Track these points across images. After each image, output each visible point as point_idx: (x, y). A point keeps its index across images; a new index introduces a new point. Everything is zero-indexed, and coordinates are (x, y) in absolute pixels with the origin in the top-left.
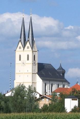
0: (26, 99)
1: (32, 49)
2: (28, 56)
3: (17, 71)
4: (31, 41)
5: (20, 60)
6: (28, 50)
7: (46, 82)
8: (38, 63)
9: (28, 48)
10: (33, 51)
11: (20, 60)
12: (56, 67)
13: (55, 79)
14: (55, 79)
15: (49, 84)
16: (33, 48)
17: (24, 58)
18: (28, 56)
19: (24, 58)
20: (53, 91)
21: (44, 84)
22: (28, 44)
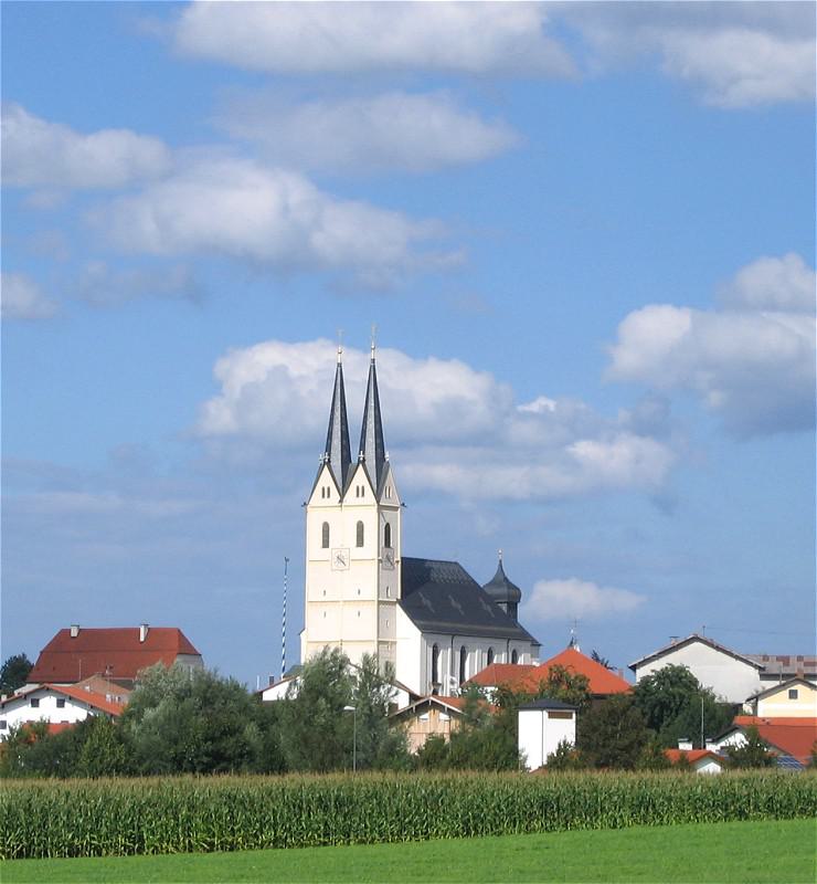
1: (378, 496)
2: (360, 527)
4: (371, 462)
5: (326, 544)
9: (360, 492)
10: (380, 508)
11: (326, 544)
15: (450, 650)
17: (343, 536)
18: (360, 527)
19: (343, 536)
22: (360, 479)
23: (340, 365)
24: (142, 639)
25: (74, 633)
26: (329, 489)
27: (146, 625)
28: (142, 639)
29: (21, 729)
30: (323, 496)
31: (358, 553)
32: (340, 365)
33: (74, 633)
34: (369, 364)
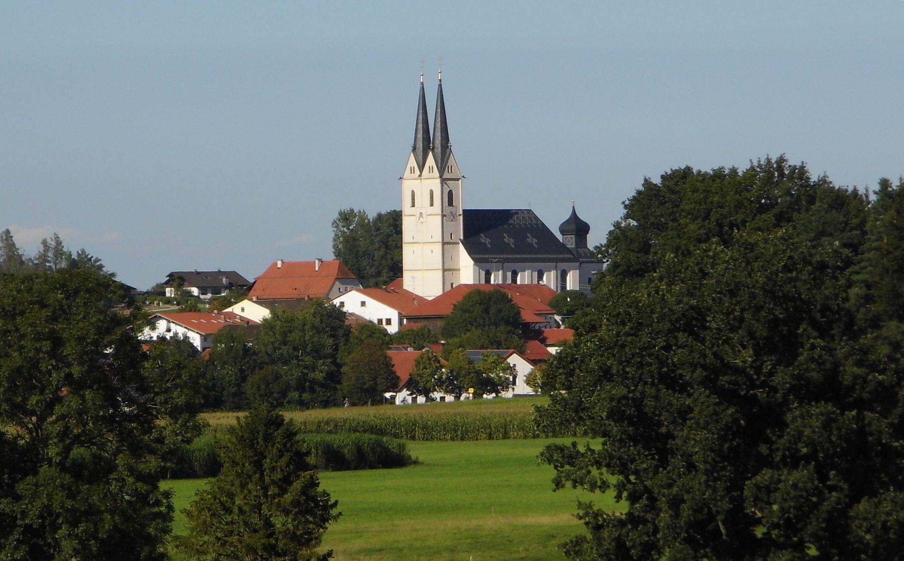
0: (493, 347)
1: (441, 171)
2: (432, 193)
3: (407, 236)
4: (438, 150)
5: (413, 205)
6: (431, 175)
7: (488, 266)
8: (464, 211)
9: (431, 170)
10: (443, 181)
11: (413, 205)
12: (678, 168)
13: (561, 256)
14: (561, 256)
15: (500, 272)
16: (444, 169)
17: (422, 200)
18: (432, 193)
19: (422, 200)
20: (454, 287)
21: (483, 273)
22: (431, 161)
23: (750, 160)
24: (317, 269)
25: (279, 264)
26: (414, 167)
27: (320, 260)
28: (317, 269)
29: (817, 185)
30: (430, 172)
31: (431, 210)
32: (750, 160)
33: (279, 264)
34: (419, 86)
